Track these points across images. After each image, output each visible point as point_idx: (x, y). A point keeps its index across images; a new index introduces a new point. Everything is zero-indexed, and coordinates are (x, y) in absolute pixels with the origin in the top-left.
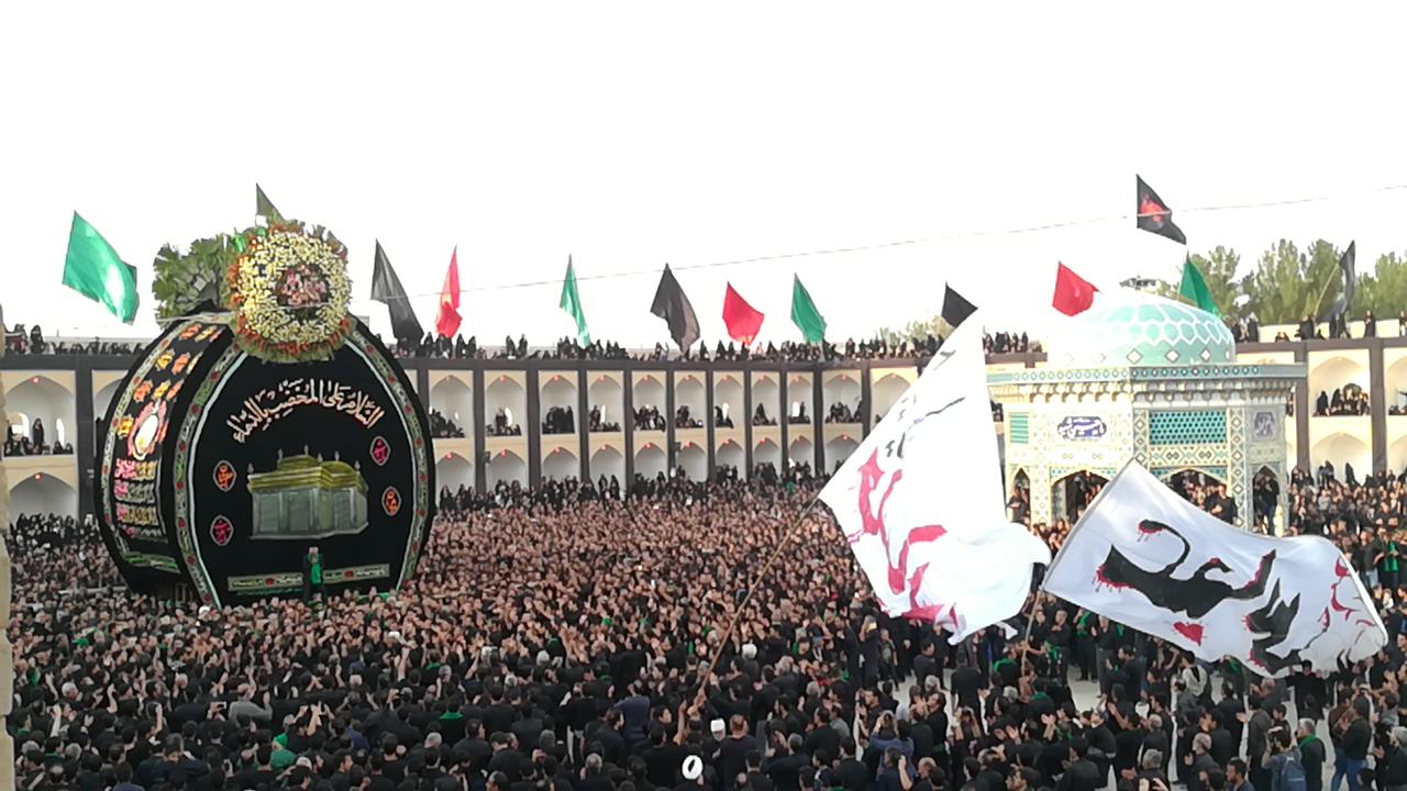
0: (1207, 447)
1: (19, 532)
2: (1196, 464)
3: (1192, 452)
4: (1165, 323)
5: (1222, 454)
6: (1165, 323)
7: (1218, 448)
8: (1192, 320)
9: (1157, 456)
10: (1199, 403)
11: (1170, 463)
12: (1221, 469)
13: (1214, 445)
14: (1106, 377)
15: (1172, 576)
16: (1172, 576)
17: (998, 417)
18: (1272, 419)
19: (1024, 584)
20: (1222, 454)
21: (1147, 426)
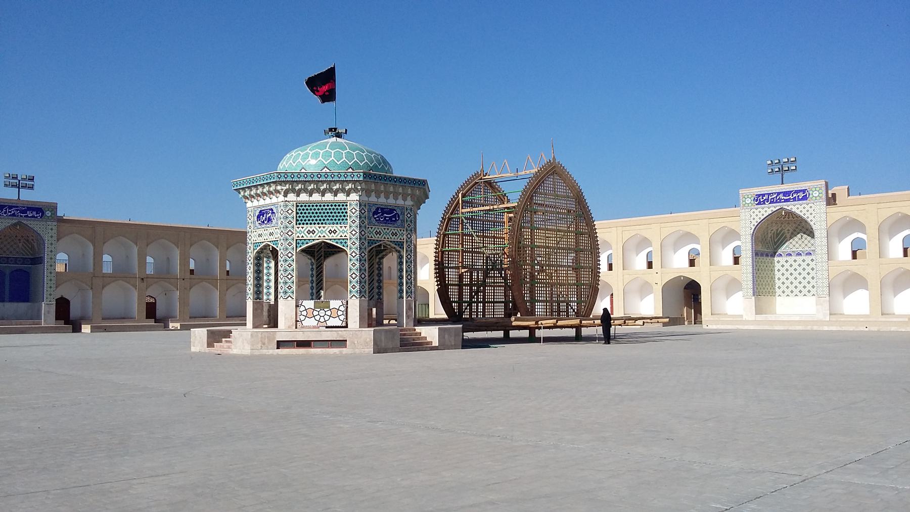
0: (334, 227)
1: (475, 297)
2: (327, 237)
3: (302, 230)
4: (365, 153)
5: (343, 232)
6: (365, 153)
7: (341, 227)
8: (292, 155)
9: (300, 232)
10: (329, 197)
11: (309, 236)
12: (345, 240)
13: (317, 226)
14: (299, 178)
15: (446, 316)
16: (446, 316)
17: (801, 195)
18: (273, 213)
19: (637, 314)
20: (343, 232)
21: (295, 213)
